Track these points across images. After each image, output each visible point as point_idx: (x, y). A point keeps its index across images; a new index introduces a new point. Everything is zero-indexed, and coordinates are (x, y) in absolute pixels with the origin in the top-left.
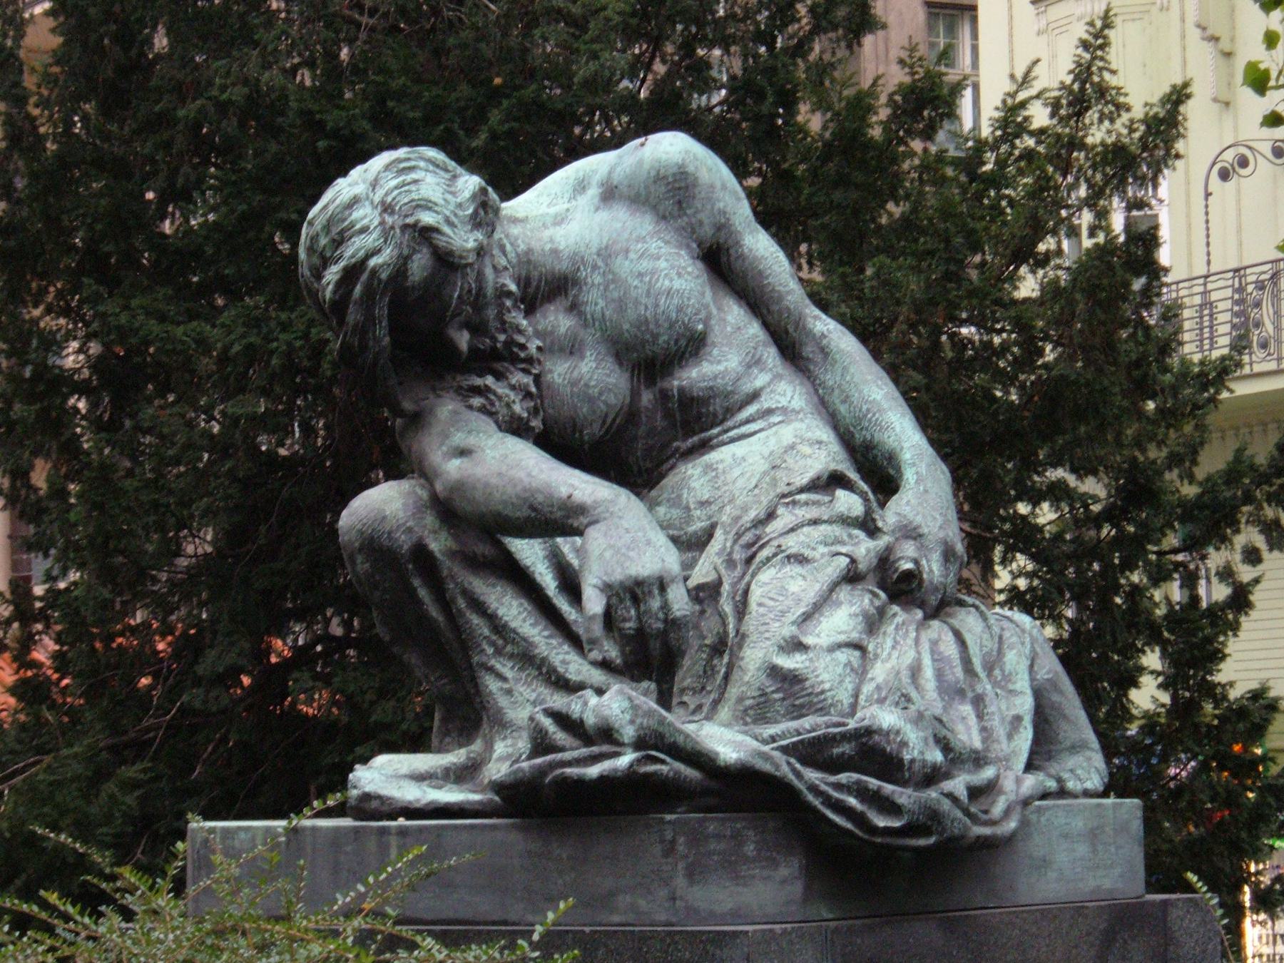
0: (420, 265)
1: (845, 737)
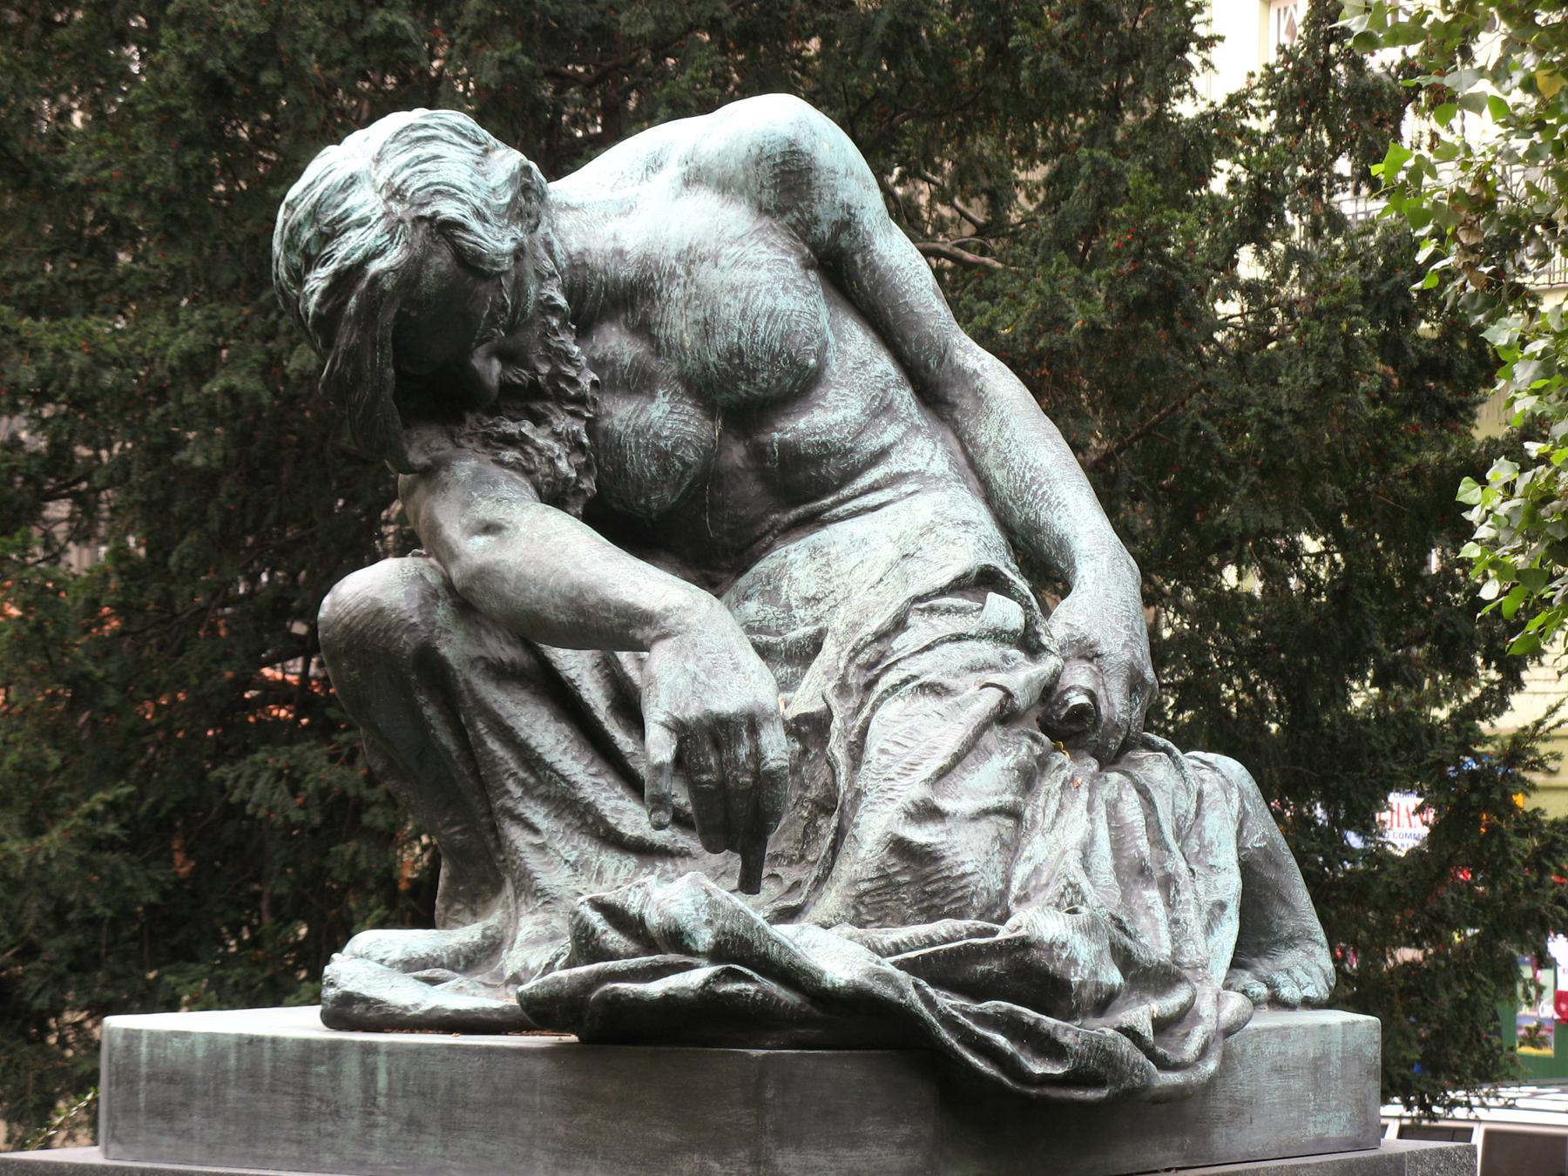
0: (442, 260)
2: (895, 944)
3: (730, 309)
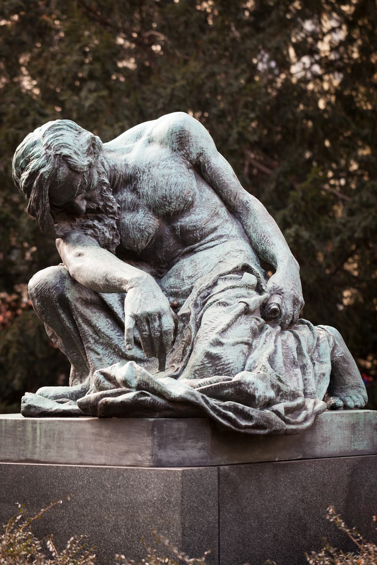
0: (63, 171)
1: (230, 386)
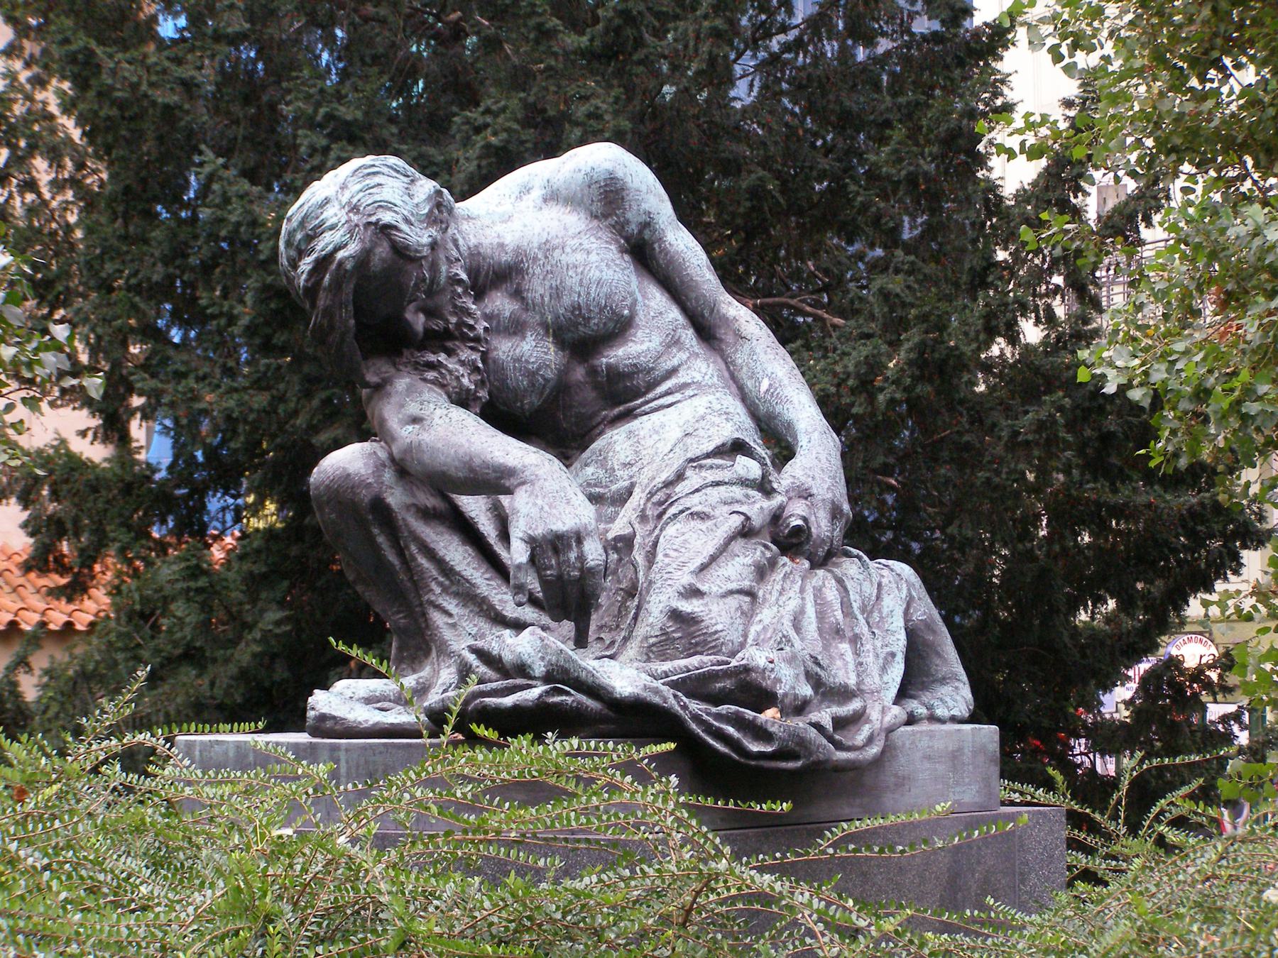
0: (383, 250)
1: (727, 674)
2: (665, 672)
3: (572, 280)
